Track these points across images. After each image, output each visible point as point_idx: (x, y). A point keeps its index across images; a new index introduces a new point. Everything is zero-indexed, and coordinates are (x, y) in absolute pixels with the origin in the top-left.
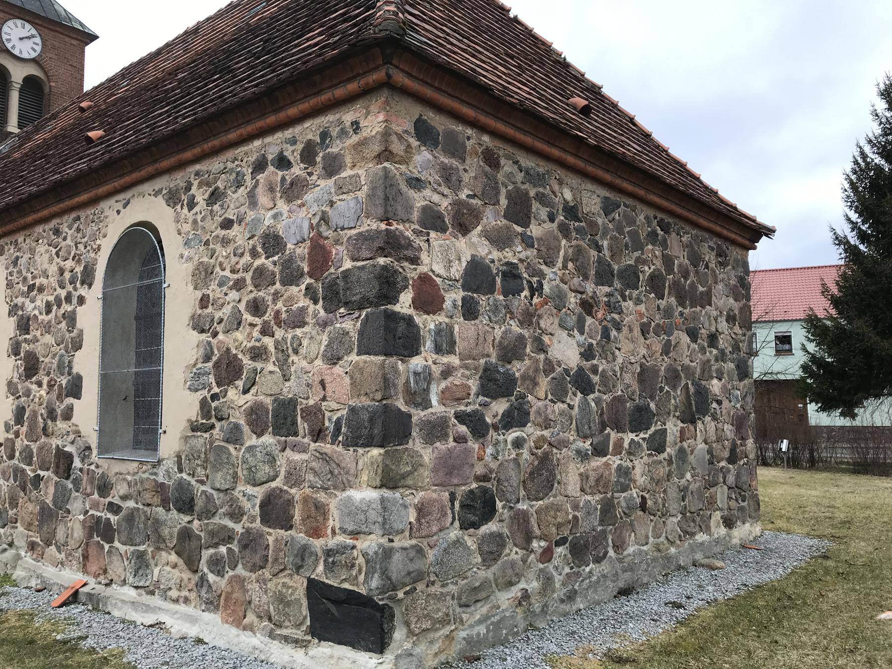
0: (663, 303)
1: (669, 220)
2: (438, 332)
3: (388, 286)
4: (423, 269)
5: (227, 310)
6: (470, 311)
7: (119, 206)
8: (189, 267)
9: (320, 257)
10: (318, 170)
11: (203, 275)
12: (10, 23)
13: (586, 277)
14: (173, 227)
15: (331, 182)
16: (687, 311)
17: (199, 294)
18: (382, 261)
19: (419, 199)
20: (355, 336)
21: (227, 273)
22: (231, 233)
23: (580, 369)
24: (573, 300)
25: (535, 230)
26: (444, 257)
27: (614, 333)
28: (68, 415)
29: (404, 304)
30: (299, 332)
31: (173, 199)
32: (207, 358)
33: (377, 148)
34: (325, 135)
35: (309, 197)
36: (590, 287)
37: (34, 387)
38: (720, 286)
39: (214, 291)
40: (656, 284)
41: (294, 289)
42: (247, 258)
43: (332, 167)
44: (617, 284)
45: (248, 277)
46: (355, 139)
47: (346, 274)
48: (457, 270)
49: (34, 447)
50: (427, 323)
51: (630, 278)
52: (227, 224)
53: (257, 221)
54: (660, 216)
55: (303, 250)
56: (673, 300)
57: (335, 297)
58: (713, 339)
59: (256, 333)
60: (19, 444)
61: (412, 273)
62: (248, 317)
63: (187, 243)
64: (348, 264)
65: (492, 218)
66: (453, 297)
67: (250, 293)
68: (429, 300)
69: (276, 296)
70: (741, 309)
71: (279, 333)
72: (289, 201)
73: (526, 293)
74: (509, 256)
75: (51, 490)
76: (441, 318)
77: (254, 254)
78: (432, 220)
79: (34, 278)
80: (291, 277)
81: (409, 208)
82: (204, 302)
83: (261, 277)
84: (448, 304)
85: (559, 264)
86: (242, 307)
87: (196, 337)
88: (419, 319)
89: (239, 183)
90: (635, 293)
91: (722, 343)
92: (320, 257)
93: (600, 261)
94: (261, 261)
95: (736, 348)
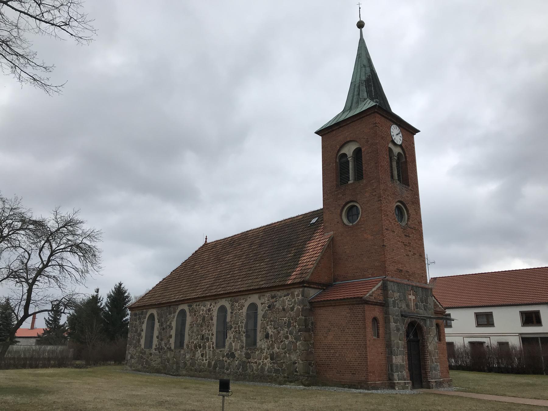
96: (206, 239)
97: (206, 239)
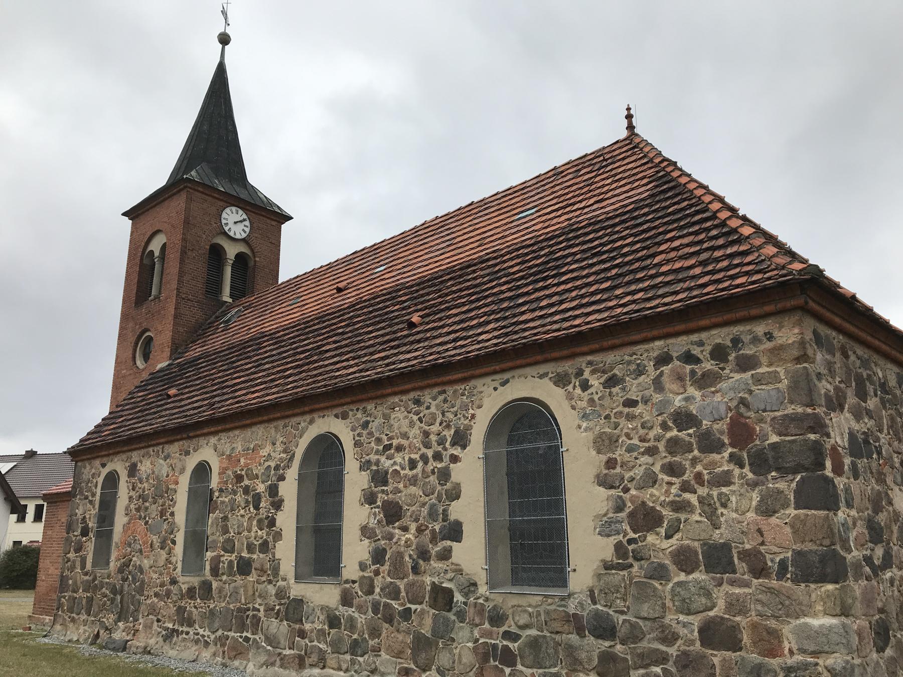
28: (445, 555)
49: (401, 584)
60: (378, 582)
75: (428, 622)
96: (629, 117)
97: (629, 117)
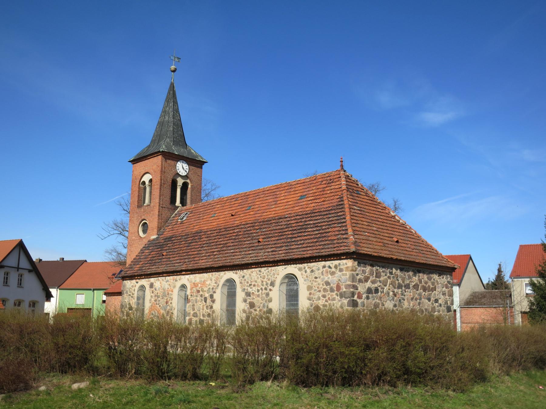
0: (418, 292)
1: (419, 269)
2: (361, 303)
3: (353, 294)
4: (359, 291)
5: (316, 297)
6: (368, 298)
7: (283, 268)
8: (306, 286)
9: (338, 288)
10: (338, 270)
11: (309, 288)
12: (179, 163)
13: (395, 288)
14: (301, 276)
15: (341, 273)
16: (426, 294)
17: (309, 292)
18: (352, 290)
19: (358, 277)
20: (346, 304)
21: (316, 288)
22: (317, 280)
23: (393, 310)
24: (391, 293)
25: (382, 279)
26: (362, 288)
27: (402, 301)
29: (356, 297)
30: (334, 302)
31: (300, 269)
32: (311, 306)
33: (351, 269)
34: (339, 264)
35: (336, 275)
36: (396, 290)
37: (253, 311)
38: (440, 285)
39: (312, 291)
40: (416, 287)
41: (333, 293)
42: (321, 286)
43: (341, 270)
44: (403, 288)
45: (322, 290)
46: (346, 266)
47: (345, 292)
48: (365, 290)
50: (359, 301)
51: (407, 286)
52: (316, 278)
53: (324, 279)
54: (417, 269)
55: (335, 286)
56: (422, 291)
57: (342, 296)
58: (436, 301)
59: (324, 301)
61: (357, 292)
62: (322, 298)
63: (305, 280)
64: (344, 290)
65: (371, 278)
66: (364, 296)
67: (322, 293)
68: (360, 297)
69: (329, 294)
70: (448, 291)
71: (329, 302)
72: (331, 275)
73: (380, 293)
74: (376, 285)
76: (362, 300)
77: (323, 284)
78: (360, 281)
79: (251, 282)
80: (332, 290)
81: (356, 280)
82: (310, 294)
83: (325, 290)
84: (363, 297)
85: (388, 285)
86: (320, 296)
87: (308, 302)
88: (358, 300)
89: (318, 270)
90: (409, 290)
91: (440, 301)
92: (338, 288)
93: (399, 283)
94: (325, 287)
95: (446, 303)
